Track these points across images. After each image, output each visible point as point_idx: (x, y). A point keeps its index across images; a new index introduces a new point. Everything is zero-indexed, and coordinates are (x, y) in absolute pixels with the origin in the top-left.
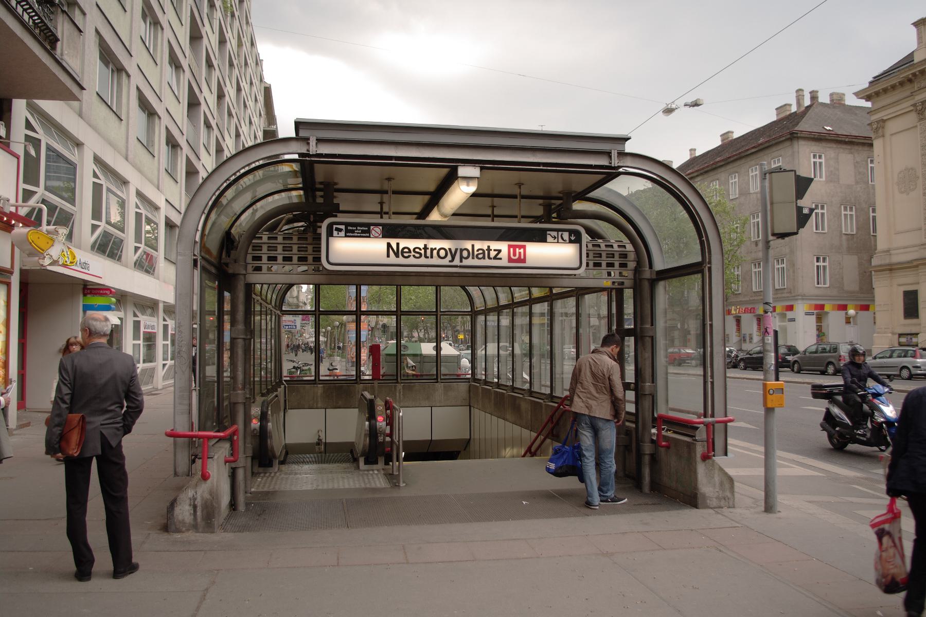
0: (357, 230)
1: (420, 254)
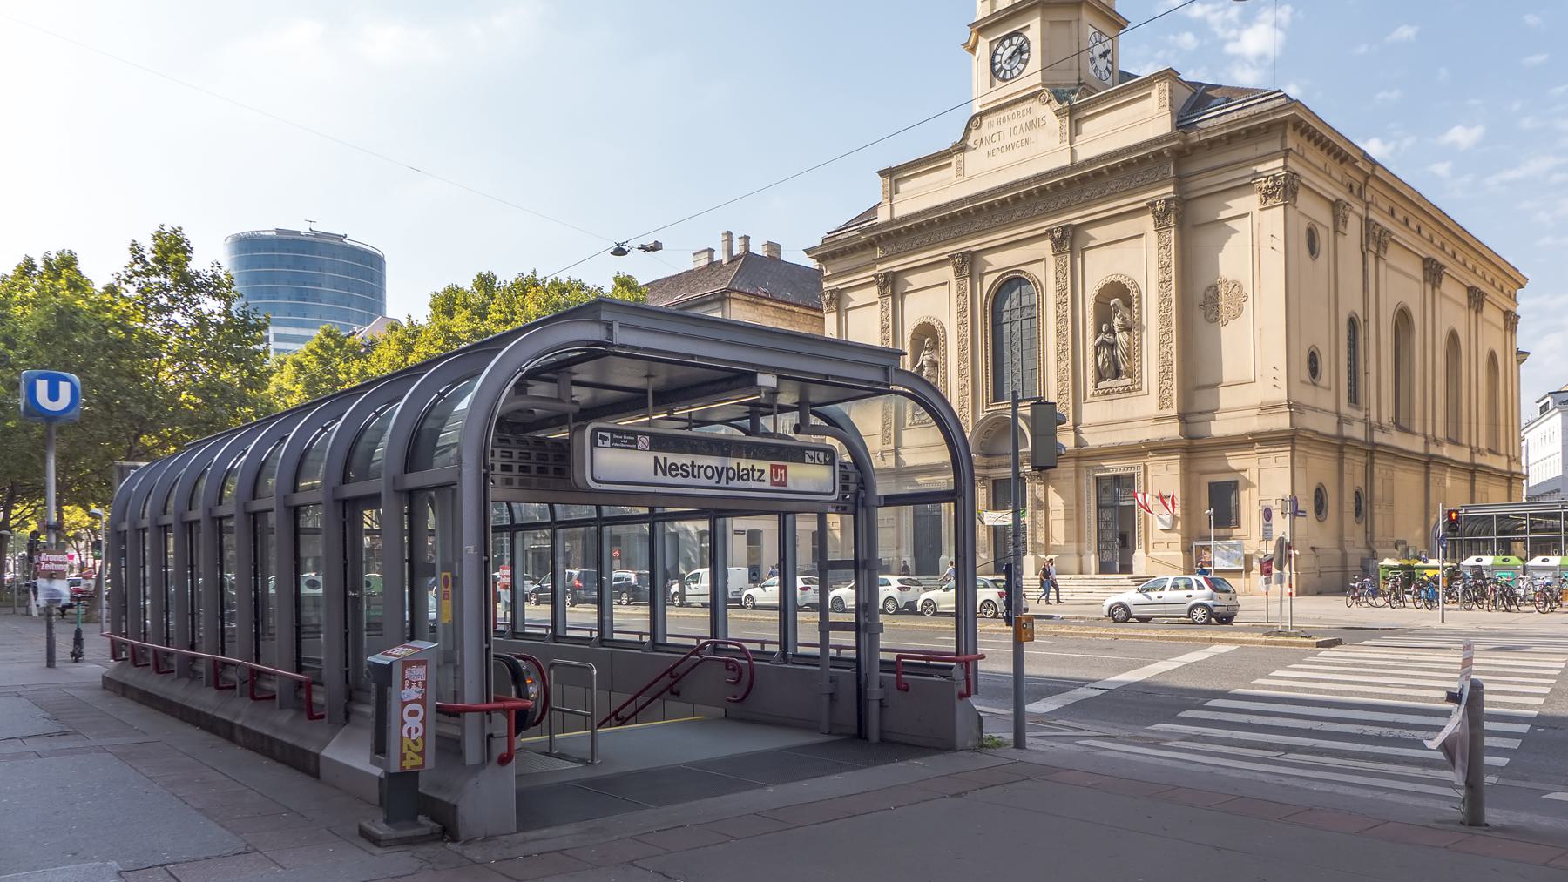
0: (623, 439)
1: (687, 472)
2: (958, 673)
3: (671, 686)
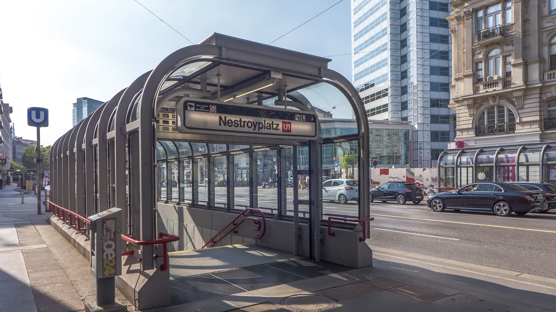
0: (201, 107)
2: (359, 227)
3: (234, 229)
